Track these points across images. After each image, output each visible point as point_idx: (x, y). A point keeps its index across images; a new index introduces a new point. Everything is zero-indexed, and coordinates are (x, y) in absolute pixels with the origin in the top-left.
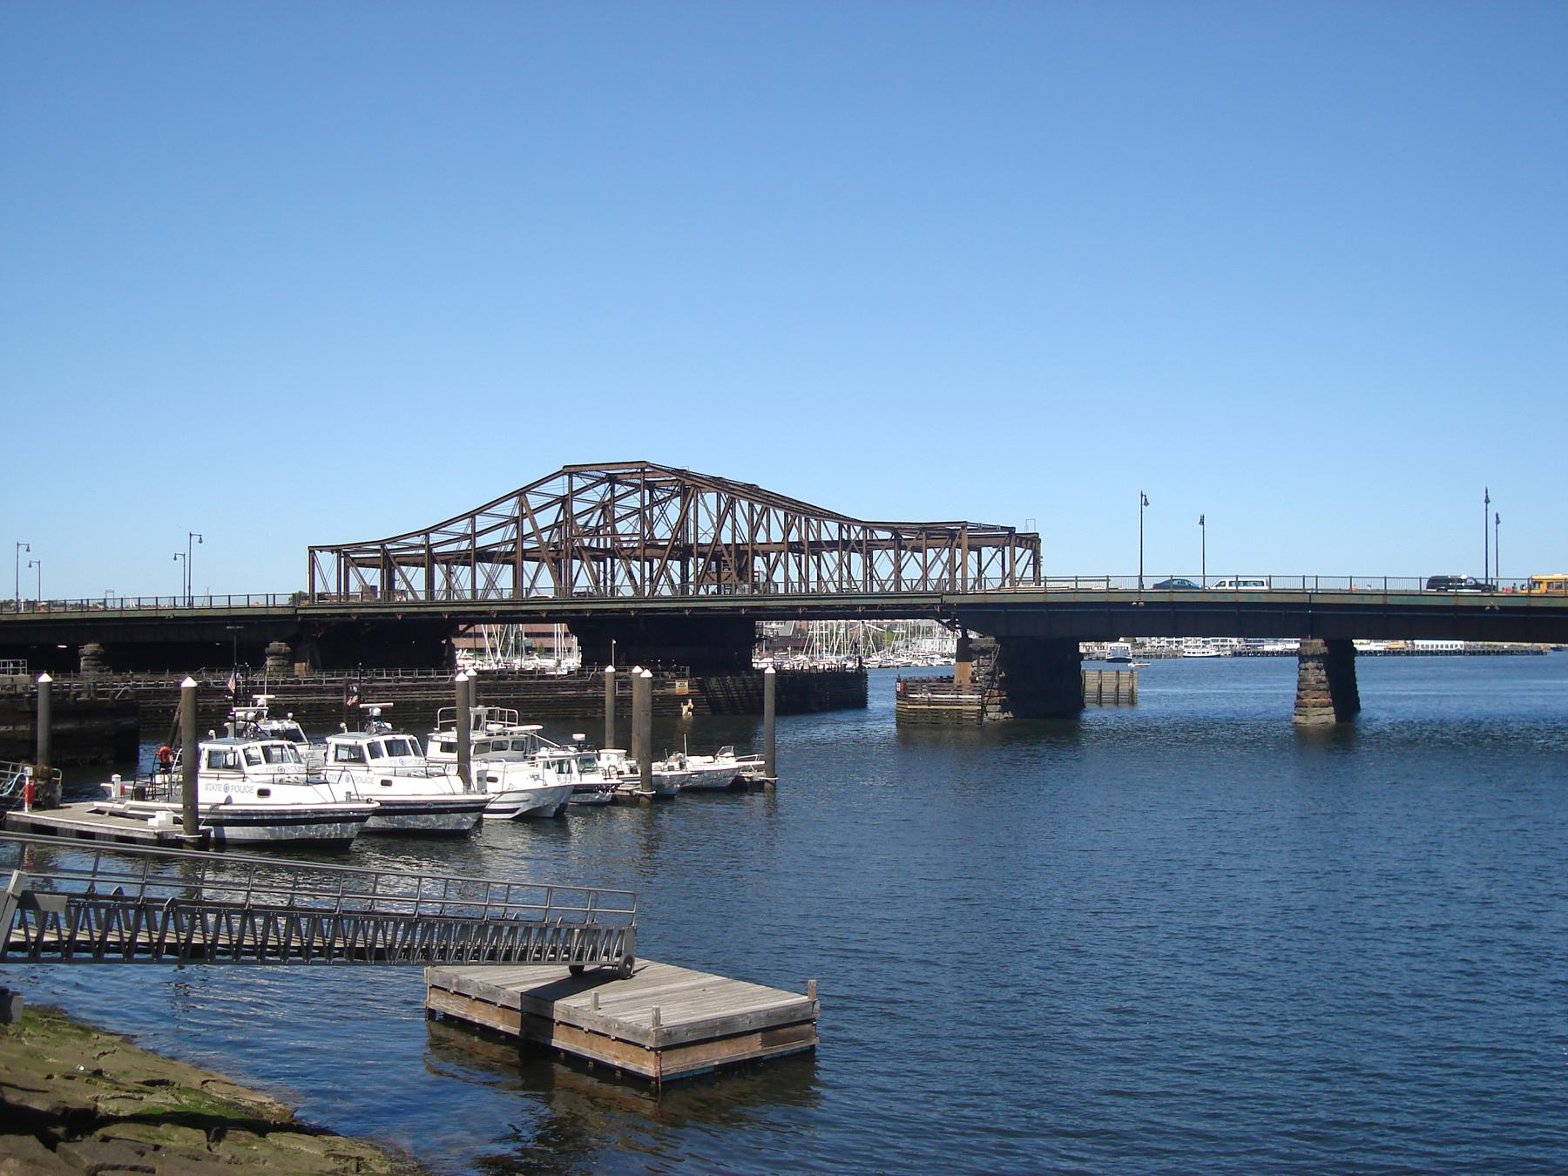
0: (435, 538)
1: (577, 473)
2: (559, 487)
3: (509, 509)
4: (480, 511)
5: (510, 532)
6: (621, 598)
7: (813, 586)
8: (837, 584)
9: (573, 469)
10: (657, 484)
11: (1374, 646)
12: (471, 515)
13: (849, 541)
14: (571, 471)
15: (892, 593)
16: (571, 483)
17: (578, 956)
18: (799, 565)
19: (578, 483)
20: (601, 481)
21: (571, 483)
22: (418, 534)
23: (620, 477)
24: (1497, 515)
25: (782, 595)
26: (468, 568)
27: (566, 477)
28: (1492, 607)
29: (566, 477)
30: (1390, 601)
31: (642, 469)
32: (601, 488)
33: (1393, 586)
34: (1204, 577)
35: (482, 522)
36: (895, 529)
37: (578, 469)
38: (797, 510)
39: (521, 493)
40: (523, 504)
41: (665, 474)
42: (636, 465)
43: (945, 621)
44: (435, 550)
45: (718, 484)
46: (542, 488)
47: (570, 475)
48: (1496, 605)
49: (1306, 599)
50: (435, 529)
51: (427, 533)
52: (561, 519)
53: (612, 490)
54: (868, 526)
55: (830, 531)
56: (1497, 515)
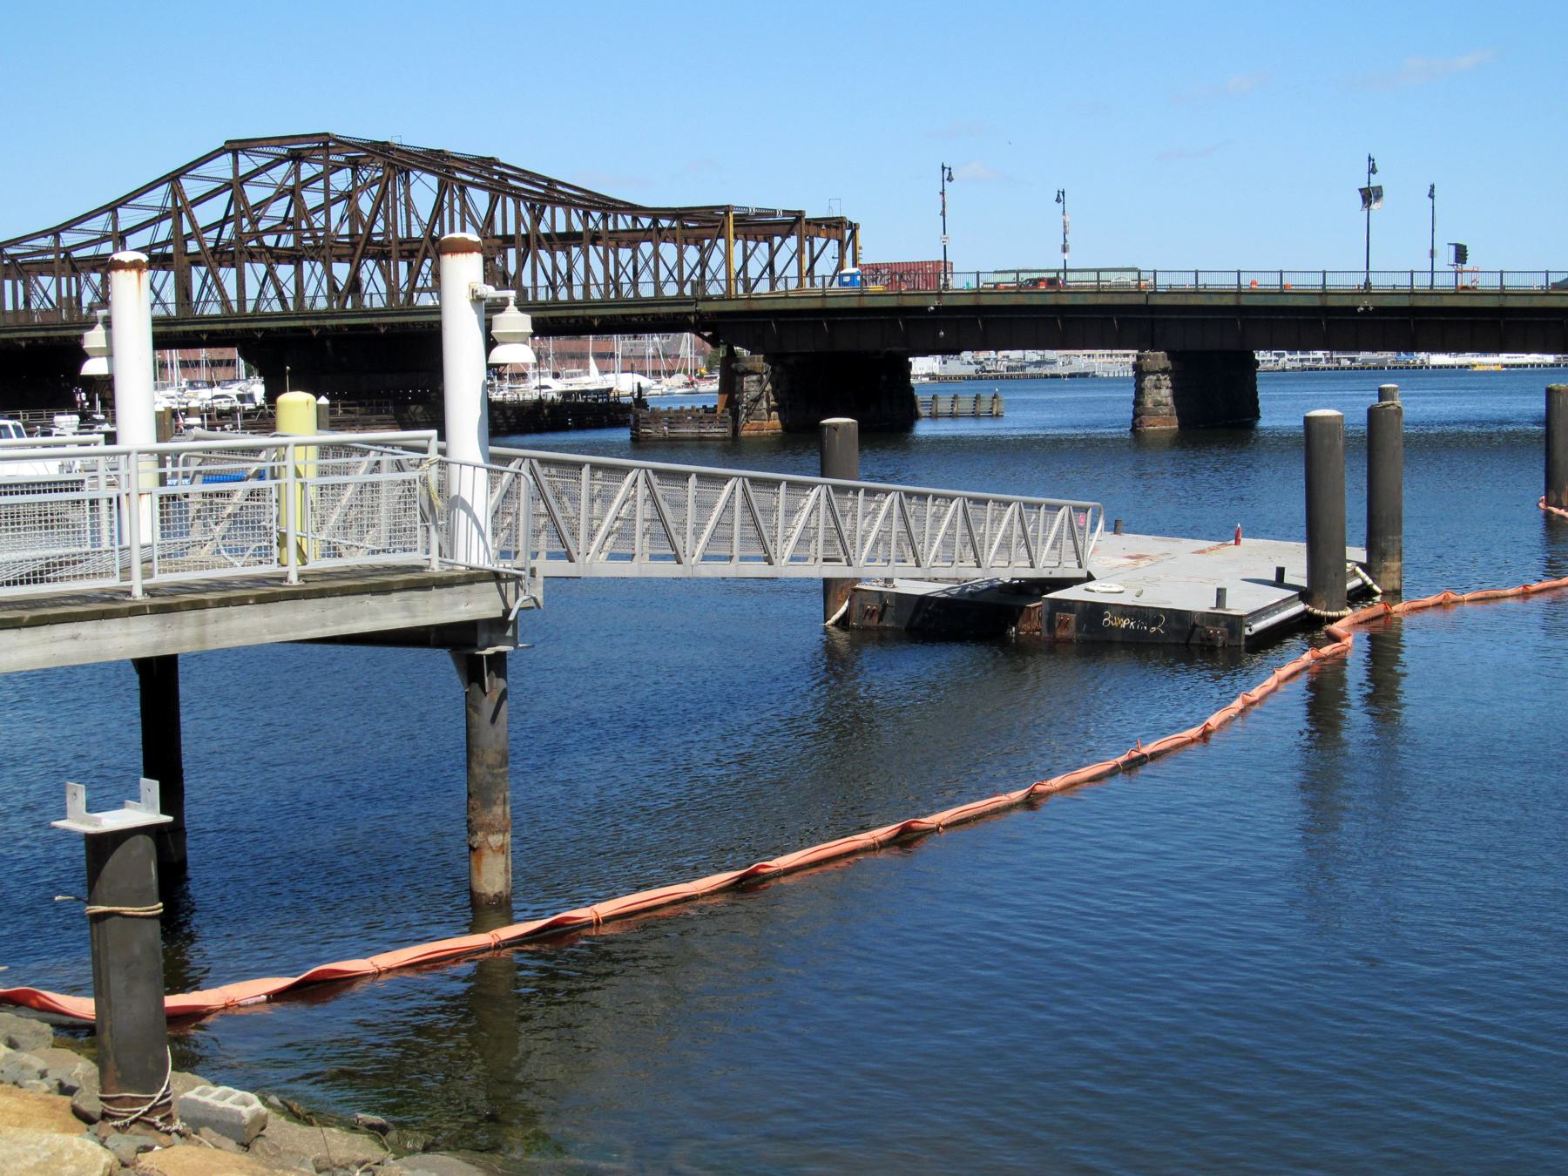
0: (68, 239)
1: (243, 150)
2: (222, 168)
3: (159, 197)
4: (123, 202)
5: (165, 230)
6: (268, 314)
7: (578, 294)
8: (602, 287)
9: (237, 146)
10: (361, 161)
11: (1290, 360)
12: (112, 208)
13: (616, 231)
14: (235, 148)
15: (630, 300)
16: (236, 162)
17: (48, 521)
18: (605, 262)
19: (246, 164)
20: (279, 161)
21: (236, 162)
22: (44, 234)
23: (306, 153)
24: (1433, 187)
25: (563, 302)
26: (234, 271)
27: (230, 155)
28: (1366, 308)
29: (230, 155)
30: (1245, 301)
31: (326, 144)
32: (286, 166)
33: (1511, 282)
34: (1368, 272)
35: (127, 218)
36: (677, 214)
37: (244, 145)
38: (549, 193)
39: (174, 178)
40: (177, 192)
41: (353, 150)
42: (316, 138)
43: (706, 334)
44: (76, 254)
45: (437, 162)
46: (202, 170)
47: (235, 154)
48: (1370, 305)
49: (1141, 300)
50: (68, 226)
51: (56, 232)
52: (232, 212)
53: (297, 173)
54: (656, 214)
55: (624, 223)
56: (1433, 187)
